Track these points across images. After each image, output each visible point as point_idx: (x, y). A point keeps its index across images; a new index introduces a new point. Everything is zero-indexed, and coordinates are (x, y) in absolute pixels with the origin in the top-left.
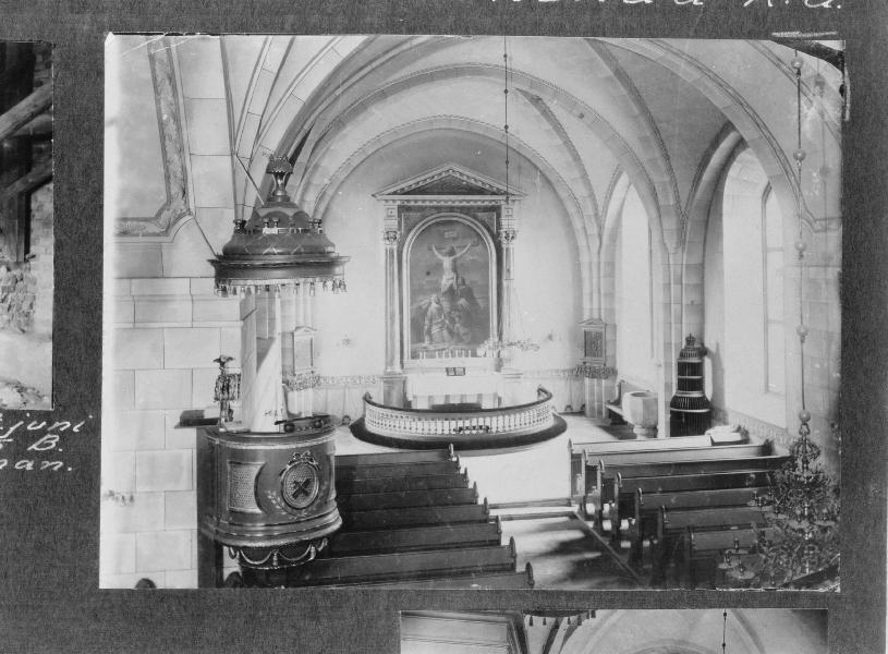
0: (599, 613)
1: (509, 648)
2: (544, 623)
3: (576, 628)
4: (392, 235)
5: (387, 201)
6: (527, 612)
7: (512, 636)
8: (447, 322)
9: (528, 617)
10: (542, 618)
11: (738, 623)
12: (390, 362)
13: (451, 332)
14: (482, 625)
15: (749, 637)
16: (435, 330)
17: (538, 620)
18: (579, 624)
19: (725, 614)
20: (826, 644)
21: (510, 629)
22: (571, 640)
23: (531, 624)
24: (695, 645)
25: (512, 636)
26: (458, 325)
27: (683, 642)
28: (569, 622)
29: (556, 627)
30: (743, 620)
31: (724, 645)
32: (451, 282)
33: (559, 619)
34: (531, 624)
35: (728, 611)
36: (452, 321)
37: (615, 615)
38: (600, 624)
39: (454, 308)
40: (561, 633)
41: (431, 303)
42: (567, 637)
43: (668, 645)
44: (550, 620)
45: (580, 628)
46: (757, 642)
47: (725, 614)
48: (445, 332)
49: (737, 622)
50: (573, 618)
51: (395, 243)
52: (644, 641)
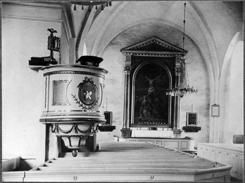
0: (113, 3)
1: (63, 23)
2: (83, 9)
3: (100, 12)
4: (128, 68)
5: (127, 53)
6: (73, 3)
7: (64, 16)
8: (150, 108)
9: (73, 5)
10: (81, 6)
11: (193, 9)
12: (126, 125)
13: (151, 113)
14: (47, 10)
15: (198, 17)
16: (144, 112)
17: (79, 7)
18: (102, 9)
19: (185, 4)
20: (242, 21)
21: (63, 12)
22: (97, 19)
23: (75, 9)
24: (168, 21)
25: (64, 16)
26: (154, 110)
27: (161, 20)
28: (96, 8)
29: (89, 10)
30: (195, 8)
31: (184, 21)
32: (152, 91)
33: (91, 6)
34: (75, 9)
35: (187, 2)
36: (152, 108)
37: (122, 4)
38: (114, 10)
39: (153, 102)
40: (92, 14)
41: (143, 100)
42: (95, 16)
43: (152, 21)
44: (86, 7)
45: (102, 11)
46: (206, 24)
47: (185, 4)
48: (149, 113)
49: (192, 9)
50: (99, 6)
51: (129, 72)
52: (139, 19)
